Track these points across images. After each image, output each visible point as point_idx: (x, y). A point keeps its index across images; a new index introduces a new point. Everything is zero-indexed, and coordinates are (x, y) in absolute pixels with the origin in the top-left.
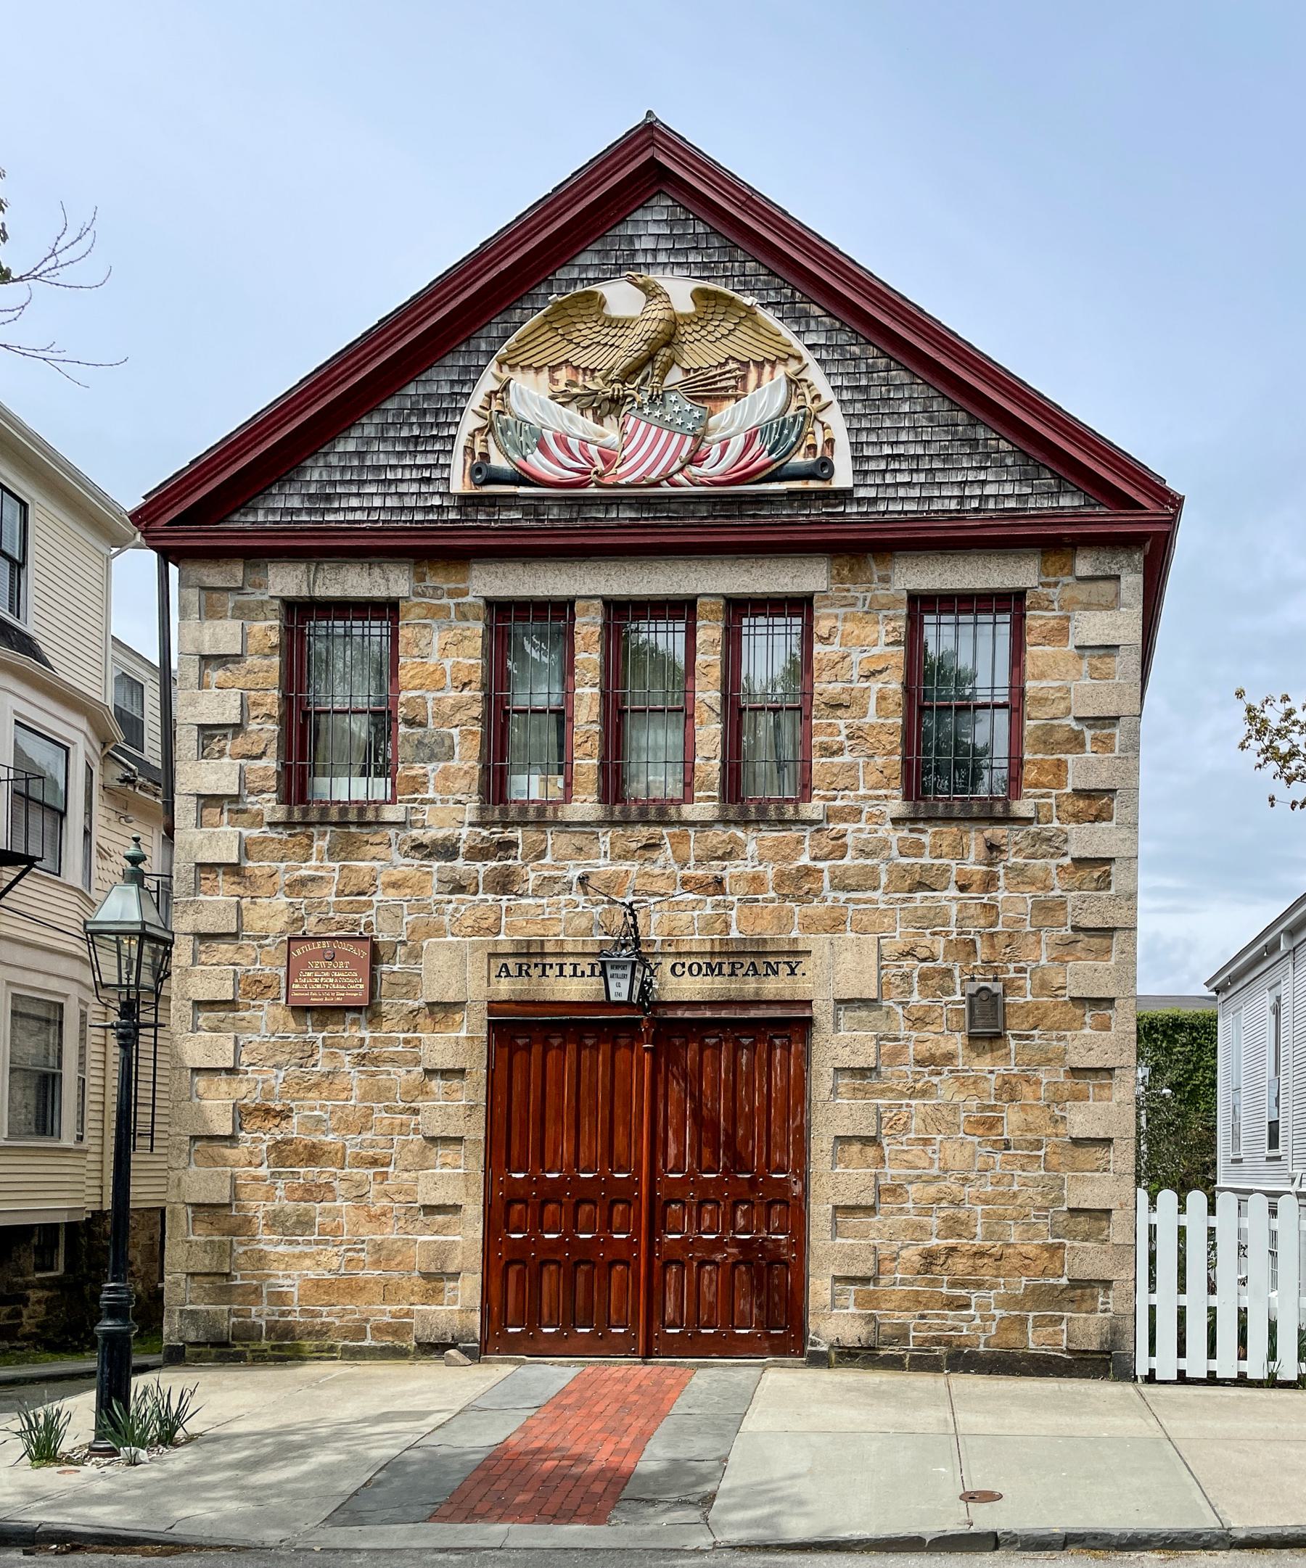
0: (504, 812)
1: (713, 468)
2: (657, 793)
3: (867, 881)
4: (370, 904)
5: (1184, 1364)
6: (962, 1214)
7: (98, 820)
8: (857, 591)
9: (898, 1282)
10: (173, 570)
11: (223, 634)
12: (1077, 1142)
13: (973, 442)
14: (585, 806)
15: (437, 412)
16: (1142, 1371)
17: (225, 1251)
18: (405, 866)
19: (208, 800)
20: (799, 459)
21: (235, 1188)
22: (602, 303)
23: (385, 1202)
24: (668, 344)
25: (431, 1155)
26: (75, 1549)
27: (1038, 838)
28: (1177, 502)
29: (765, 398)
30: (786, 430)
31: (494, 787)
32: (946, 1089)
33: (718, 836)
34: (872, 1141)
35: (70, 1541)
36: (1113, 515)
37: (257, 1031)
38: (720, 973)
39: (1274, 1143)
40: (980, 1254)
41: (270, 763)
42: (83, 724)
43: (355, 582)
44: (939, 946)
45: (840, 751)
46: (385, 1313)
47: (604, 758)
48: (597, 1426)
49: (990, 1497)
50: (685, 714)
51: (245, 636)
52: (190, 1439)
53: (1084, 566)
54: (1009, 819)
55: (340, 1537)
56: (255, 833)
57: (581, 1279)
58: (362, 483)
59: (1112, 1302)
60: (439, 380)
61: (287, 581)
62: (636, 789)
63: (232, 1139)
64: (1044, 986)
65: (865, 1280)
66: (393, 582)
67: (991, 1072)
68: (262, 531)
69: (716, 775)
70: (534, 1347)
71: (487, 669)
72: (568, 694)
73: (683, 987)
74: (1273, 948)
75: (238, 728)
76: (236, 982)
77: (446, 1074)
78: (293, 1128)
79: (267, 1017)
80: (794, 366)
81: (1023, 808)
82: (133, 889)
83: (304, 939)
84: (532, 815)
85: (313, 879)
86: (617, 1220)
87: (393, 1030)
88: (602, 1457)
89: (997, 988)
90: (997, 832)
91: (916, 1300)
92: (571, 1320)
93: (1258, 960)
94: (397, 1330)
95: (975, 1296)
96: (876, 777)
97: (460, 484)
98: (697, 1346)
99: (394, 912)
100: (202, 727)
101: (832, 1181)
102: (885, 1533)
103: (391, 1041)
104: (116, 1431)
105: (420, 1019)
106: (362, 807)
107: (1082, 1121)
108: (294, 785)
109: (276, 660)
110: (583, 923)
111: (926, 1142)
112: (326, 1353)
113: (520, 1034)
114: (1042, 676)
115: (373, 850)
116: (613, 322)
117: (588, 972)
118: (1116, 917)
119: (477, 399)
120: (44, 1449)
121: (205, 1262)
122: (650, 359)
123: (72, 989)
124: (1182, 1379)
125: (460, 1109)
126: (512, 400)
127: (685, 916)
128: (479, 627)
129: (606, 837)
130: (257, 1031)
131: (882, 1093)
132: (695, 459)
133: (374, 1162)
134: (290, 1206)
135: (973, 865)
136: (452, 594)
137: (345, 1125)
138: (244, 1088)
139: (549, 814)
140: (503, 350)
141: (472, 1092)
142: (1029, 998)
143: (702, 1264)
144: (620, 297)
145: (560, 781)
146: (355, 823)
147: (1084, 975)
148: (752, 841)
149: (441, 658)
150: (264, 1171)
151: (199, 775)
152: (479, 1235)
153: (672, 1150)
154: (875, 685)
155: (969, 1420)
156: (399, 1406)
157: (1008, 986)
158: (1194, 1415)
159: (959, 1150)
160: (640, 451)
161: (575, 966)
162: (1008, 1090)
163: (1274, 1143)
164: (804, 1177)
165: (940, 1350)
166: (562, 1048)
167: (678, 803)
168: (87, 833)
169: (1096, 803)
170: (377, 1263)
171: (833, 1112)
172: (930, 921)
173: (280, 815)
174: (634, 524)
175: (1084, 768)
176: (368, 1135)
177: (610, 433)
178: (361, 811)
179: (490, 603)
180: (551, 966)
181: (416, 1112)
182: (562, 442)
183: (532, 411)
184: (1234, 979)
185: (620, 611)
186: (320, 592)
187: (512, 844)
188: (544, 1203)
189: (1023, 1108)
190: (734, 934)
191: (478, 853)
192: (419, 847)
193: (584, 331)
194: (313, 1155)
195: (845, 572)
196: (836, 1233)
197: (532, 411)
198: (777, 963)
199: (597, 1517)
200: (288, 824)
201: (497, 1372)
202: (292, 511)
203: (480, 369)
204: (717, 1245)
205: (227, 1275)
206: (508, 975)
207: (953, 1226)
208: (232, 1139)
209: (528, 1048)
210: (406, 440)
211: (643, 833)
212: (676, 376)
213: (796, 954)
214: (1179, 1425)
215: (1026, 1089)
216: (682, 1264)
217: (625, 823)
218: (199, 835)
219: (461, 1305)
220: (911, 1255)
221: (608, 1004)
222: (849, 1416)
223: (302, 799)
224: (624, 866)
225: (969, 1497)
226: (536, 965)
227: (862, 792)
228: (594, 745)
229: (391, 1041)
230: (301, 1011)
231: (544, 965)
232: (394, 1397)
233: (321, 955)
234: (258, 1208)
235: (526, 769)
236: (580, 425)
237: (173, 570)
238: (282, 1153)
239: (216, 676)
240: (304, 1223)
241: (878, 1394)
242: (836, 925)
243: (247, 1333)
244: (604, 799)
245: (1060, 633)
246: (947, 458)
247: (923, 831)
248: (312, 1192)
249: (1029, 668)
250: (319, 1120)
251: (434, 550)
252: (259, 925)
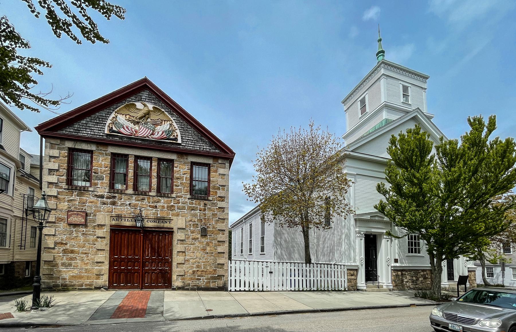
0: (114, 191)
1: (156, 136)
2: (144, 190)
3: (183, 208)
4: (85, 205)
5: (245, 288)
6: (200, 264)
7: (15, 183)
8: (182, 160)
9: (188, 276)
10: (44, 139)
11: (55, 152)
12: (219, 253)
13: (202, 139)
14: (130, 191)
15: (102, 119)
16: (229, 290)
17: (52, 270)
18: (93, 199)
19: (50, 183)
20: (171, 137)
21: (54, 258)
22: (136, 105)
23: (88, 261)
24: (148, 114)
25: (98, 252)
26: (36, 327)
27: (213, 203)
28: (235, 154)
29: (166, 126)
30: (170, 132)
31: (112, 186)
32: (197, 244)
33: (156, 198)
34: (184, 252)
35: (27, 326)
37: (60, 228)
39: (242, 252)
40: (203, 271)
41: (65, 177)
42: (14, 164)
43: (84, 146)
44: (196, 220)
45: (179, 186)
46: (88, 282)
47: (134, 183)
48: (137, 301)
49: (211, 310)
50: (150, 176)
51: (60, 153)
52: (52, 306)
53: (220, 161)
54: (208, 200)
55: (93, 322)
56: (61, 190)
57: (129, 275)
58: (86, 129)
59: (224, 279)
60: (103, 113)
61: (69, 144)
62: (140, 189)
63: (54, 248)
64: (214, 227)
65: (182, 276)
66: (93, 148)
68: (65, 135)
69: (156, 188)
70: (119, 288)
71: (111, 165)
72: (127, 171)
73: (150, 224)
74: (242, 221)
75: (57, 170)
76: (56, 218)
77: (101, 238)
78: (68, 247)
79: (62, 226)
80: (171, 122)
81: (210, 198)
82: (43, 201)
83: (71, 211)
84: (119, 192)
85: (73, 200)
86: (136, 265)
87: (90, 229)
88: (140, 307)
89: (206, 227)
90: (206, 202)
91: (191, 279)
92: (127, 283)
93: (239, 223)
94: (91, 285)
95: (202, 278)
96: (185, 191)
97: (106, 132)
98: (151, 287)
99: (91, 207)
100: (49, 169)
101: (177, 259)
102: (195, 317)
103: (90, 231)
104: (36, 304)
105: (96, 227)
106: (84, 187)
107: (220, 249)
108: (70, 181)
109: (66, 158)
110: (130, 212)
111: (194, 252)
112: (74, 289)
113: (117, 233)
114: (213, 178)
115: (87, 196)
116: (138, 109)
118: (225, 217)
119: (111, 118)
120: (21, 308)
121: (47, 272)
122: (145, 116)
123: (9, 217)
124: (236, 291)
125: (105, 244)
126: (118, 119)
127: (150, 212)
128: (110, 157)
129: (134, 197)
130: (60, 228)
131: (186, 244)
132: (152, 134)
133: (86, 253)
134: (67, 261)
135: (202, 207)
136: (104, 151)
137: (79, 246)
138: (57, 239)
139: (123, 192)
140: (116, 110)
141: (107, 241)
143: (152, 273)
144: (139, 105)
145: (125, 186)
146: (82, 191)
147: (220, 226)
148: (163, 200)
149: (102, 162)
150: (61, 254)
151: (47, 178)
152: (108, 267)
153: (147, 253)
154: (185, 176)
155: (203, 298)
156: (94, 299)
157: (208, 227)
158: (240, 297)
159: (199, 254)
160: (142, 131)
162: (208, 244)
163: (242, 252)
164: (172, 258)
165: (196, 287)
166: (125, 234)
167: (149, 192)
168: (13, 185)
169: (222, 199)
170: (86, 272)
171: (177, 247)
172: (195, 215)
173: (66, 187)
174: (141, 143)
175: (220, 193)
176: (84, 248)
177: (137, 127)
178: (84, 188)
179: (112, 153)
181: (95, 244)
182: (127, 128)
183: (121, 121)
184: (235, 226)
185: (137, 158)
186: (76, 147)
187: (115, 197)
188: (128, 262)
190: (159, 216)
191: (108, 198)
192: (96, 196)
193: (132, 110)
194: (72, 252)
196: (177, 267)
197: (121, 121)
199: (142, 316)
200: (68, 189)
201: (111, 293)
202: (71, 132)
203: (111, 113)
204: (155, 270)
205: (52, 275)
207: (198, 267)
208: (54, 248)
209: (118, 234)
210: (96, 123)
211: (142, 197)
212: (149, 120)
213: (170, 220)
214: (237, 298)
215: (211, 244)
216: (148, 273)
217: (138, 195)
218: (48, 190)
219: (104, 280)
220: (191, 271)
221: (136, 227)
222: (183, 298)
223: (71, 185)
224: (138, 202)
225: (207, 310)
228: (132, 180)
229: (90, 231)
230: (70, 225)
232: (92, 297)
233: (75, 214)
234: (59, 262)
235: (117, 183)
236: (131, 125)
237: (44, 139)
238: (65, 251)
239: (53, 160)
240: (70, 265)
241: (186, 295)
242: (178, 215)
243: (57, 286)
244: (134, 190)
245: (216, 171)
246: (197, 141)
248: (71, 259)
249: (211, 176)
250: (74, 245)
251: (102, 143)
252: (61, 208)
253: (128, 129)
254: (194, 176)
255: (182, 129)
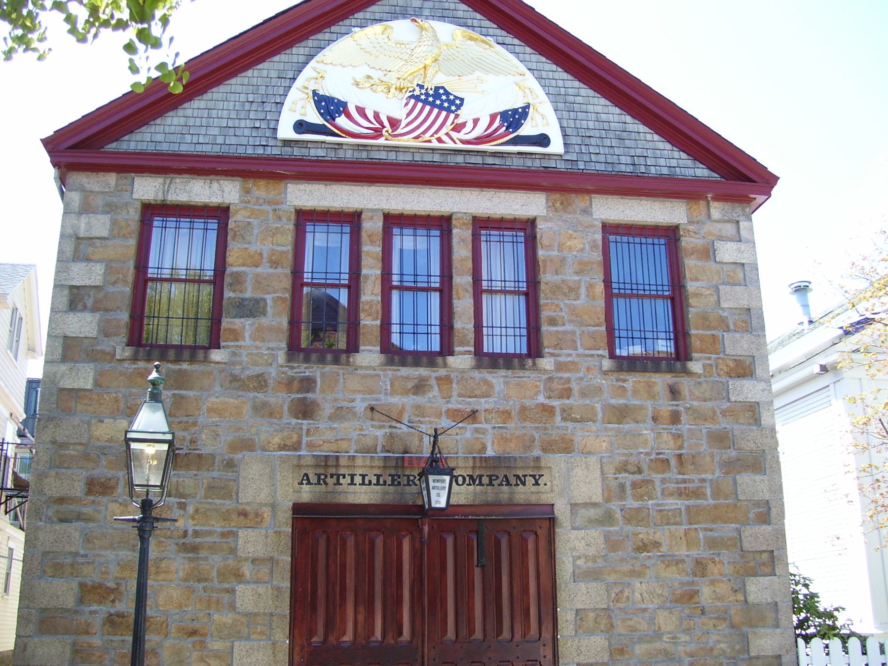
36: (740, 179)
38: (480, 484)
61: (148, 188)
67: (688, 556)
113: (317, 526)
117: (374, 481)
142: (711, 501)
161: (363, 476)
180: (344, 477)
189: (713, 582)
195: (558, 205)
198: (525, 476)
206: (309, 483)
226: (332, 476)
227: (580, 351)
231: (338, 476)
247: (624, 381)
253: (365, 117)
254: (153, 262)
255: (557, 99)
